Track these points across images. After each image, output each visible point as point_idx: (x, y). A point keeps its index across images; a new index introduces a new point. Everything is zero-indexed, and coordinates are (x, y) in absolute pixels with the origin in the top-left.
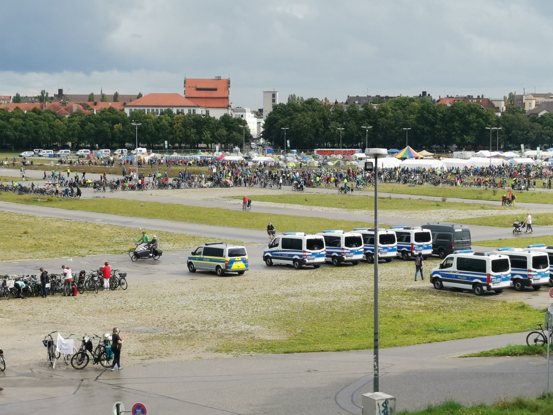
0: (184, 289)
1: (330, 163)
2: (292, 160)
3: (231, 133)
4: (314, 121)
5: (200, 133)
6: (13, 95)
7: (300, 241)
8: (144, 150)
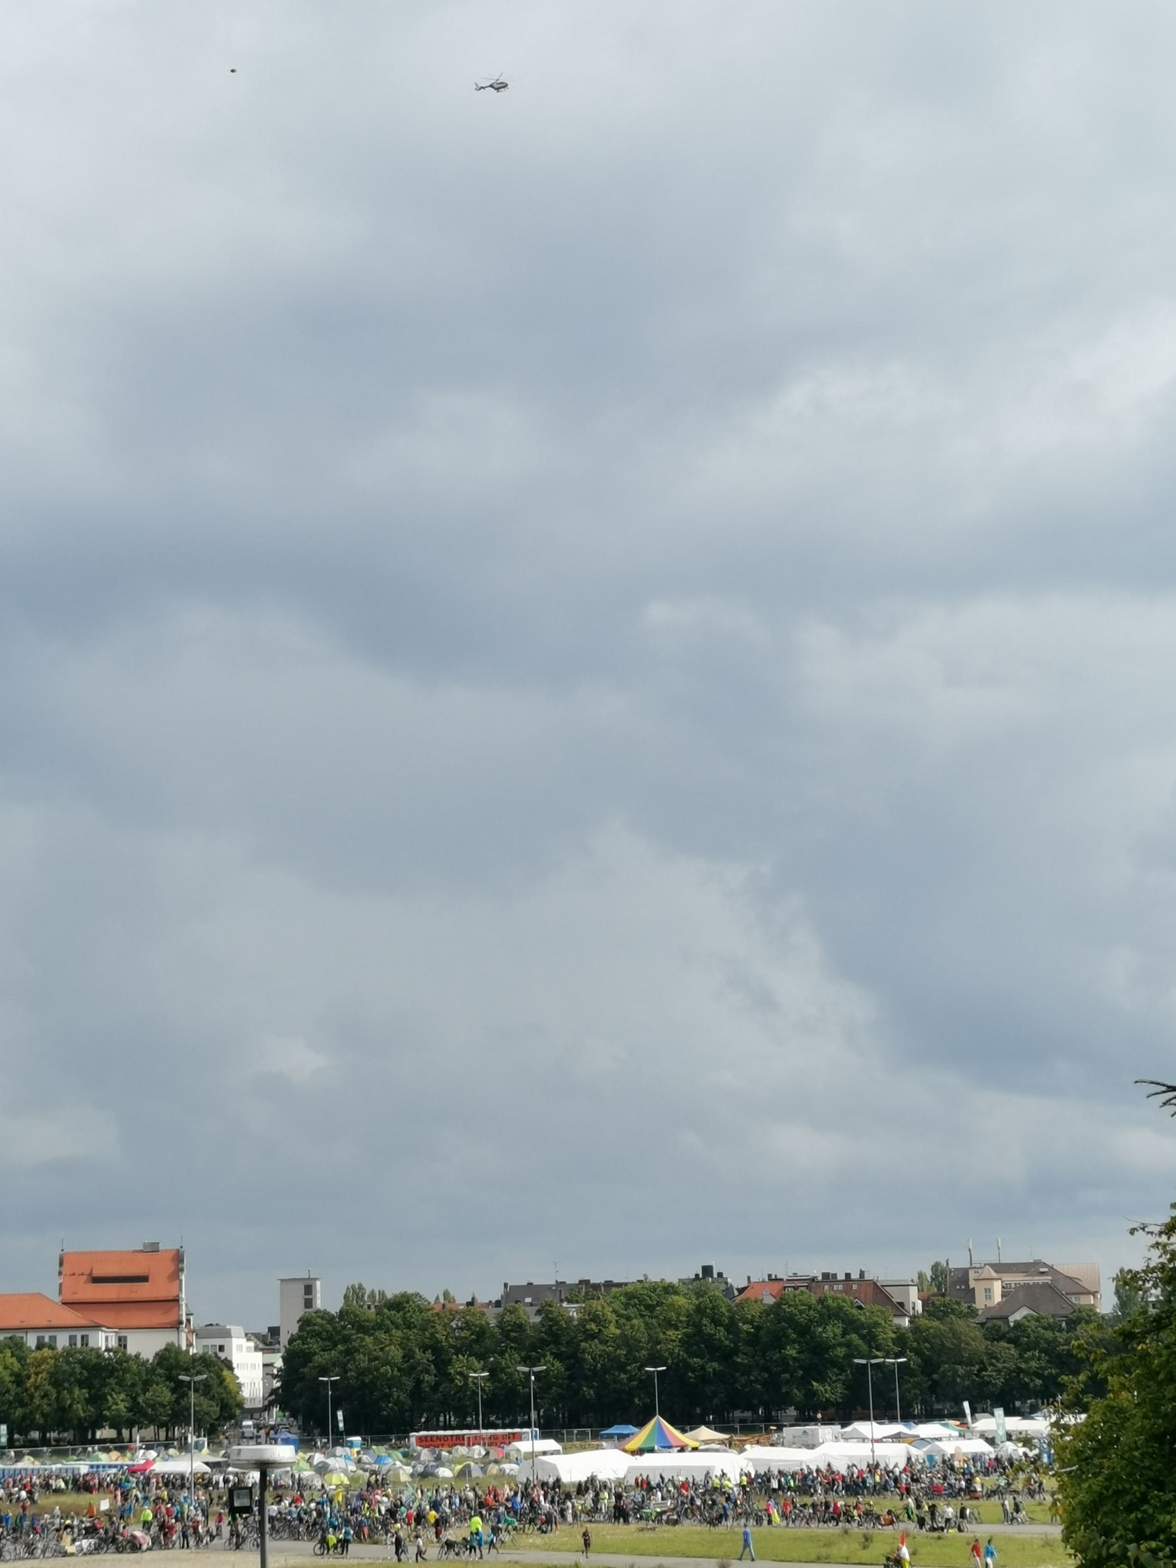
2: (342, 1466)
3: (187, 1396)
4: (408, 1356)
5: (96, 1399)
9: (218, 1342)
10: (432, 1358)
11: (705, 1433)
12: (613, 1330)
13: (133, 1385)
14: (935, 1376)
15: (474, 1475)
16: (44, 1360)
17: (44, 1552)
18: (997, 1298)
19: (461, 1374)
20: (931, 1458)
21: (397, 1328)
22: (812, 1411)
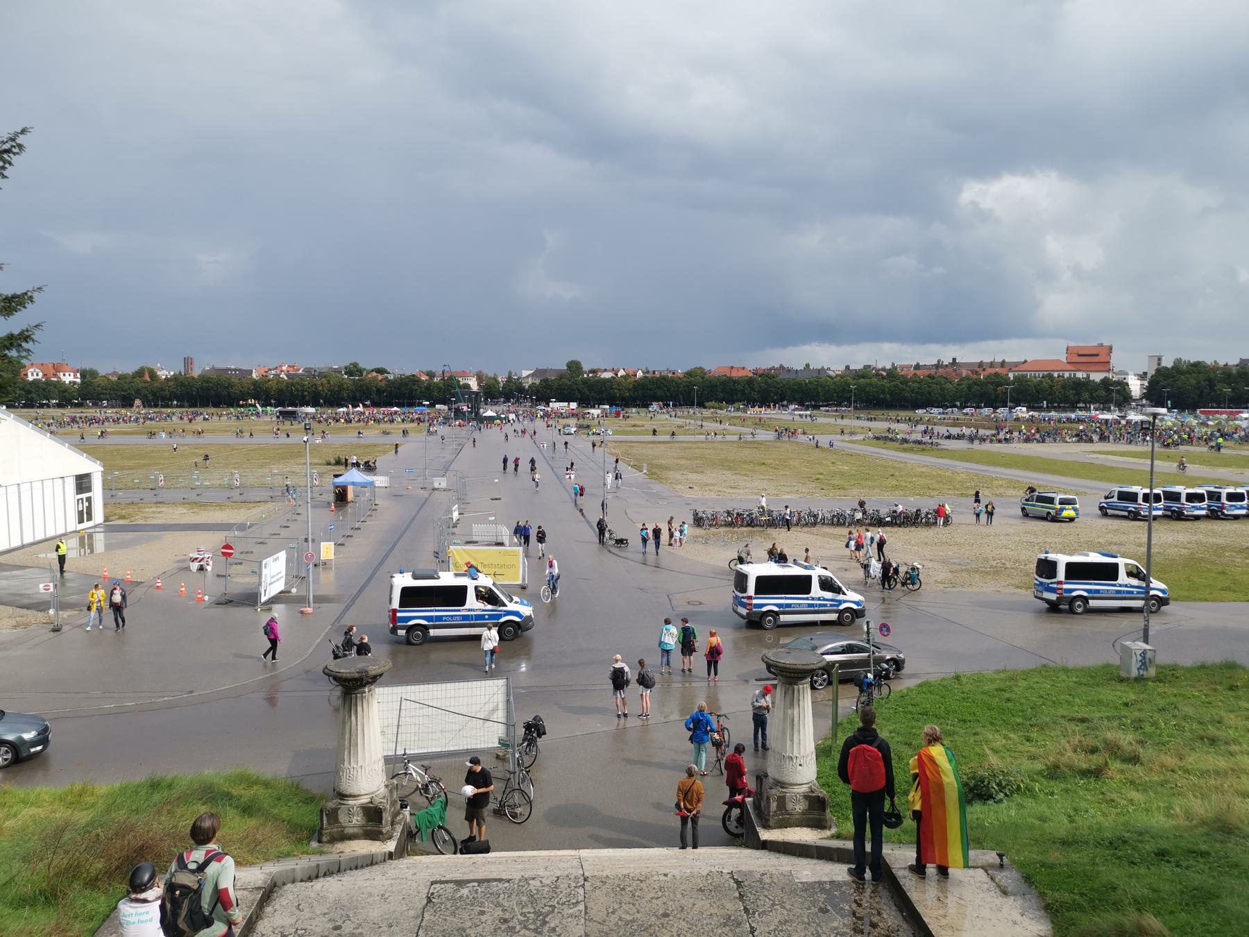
0: (1011, 531)
1: (1210, 423)
2: (1167, 417)
3: (1114, 394)
5: (1078, 394)
6: (914, 364)
7: (1136, 495)
8: (1024, 409)
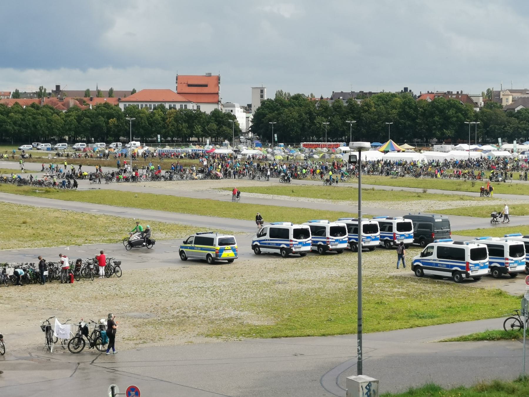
0: (176, 276)
1: (315, 156)
2: (279, 153)
3: (221, 127)
4: (300, 116)
5: (191, 127)
6: (13, 91)
7: (287, 231)
8: (138, 144)
9: (230, 109)
10: (308, 117)
11: (406, 146)
12: (373, 109)
13: (204, 123)
14: (488, 129)
15: (326, 158)
16: (172, 113)
17: (186, 178)
18: (510, 102)
19: (318, 123)
20: (489, 157)
21: (296, 106)
22: (443, 140)
